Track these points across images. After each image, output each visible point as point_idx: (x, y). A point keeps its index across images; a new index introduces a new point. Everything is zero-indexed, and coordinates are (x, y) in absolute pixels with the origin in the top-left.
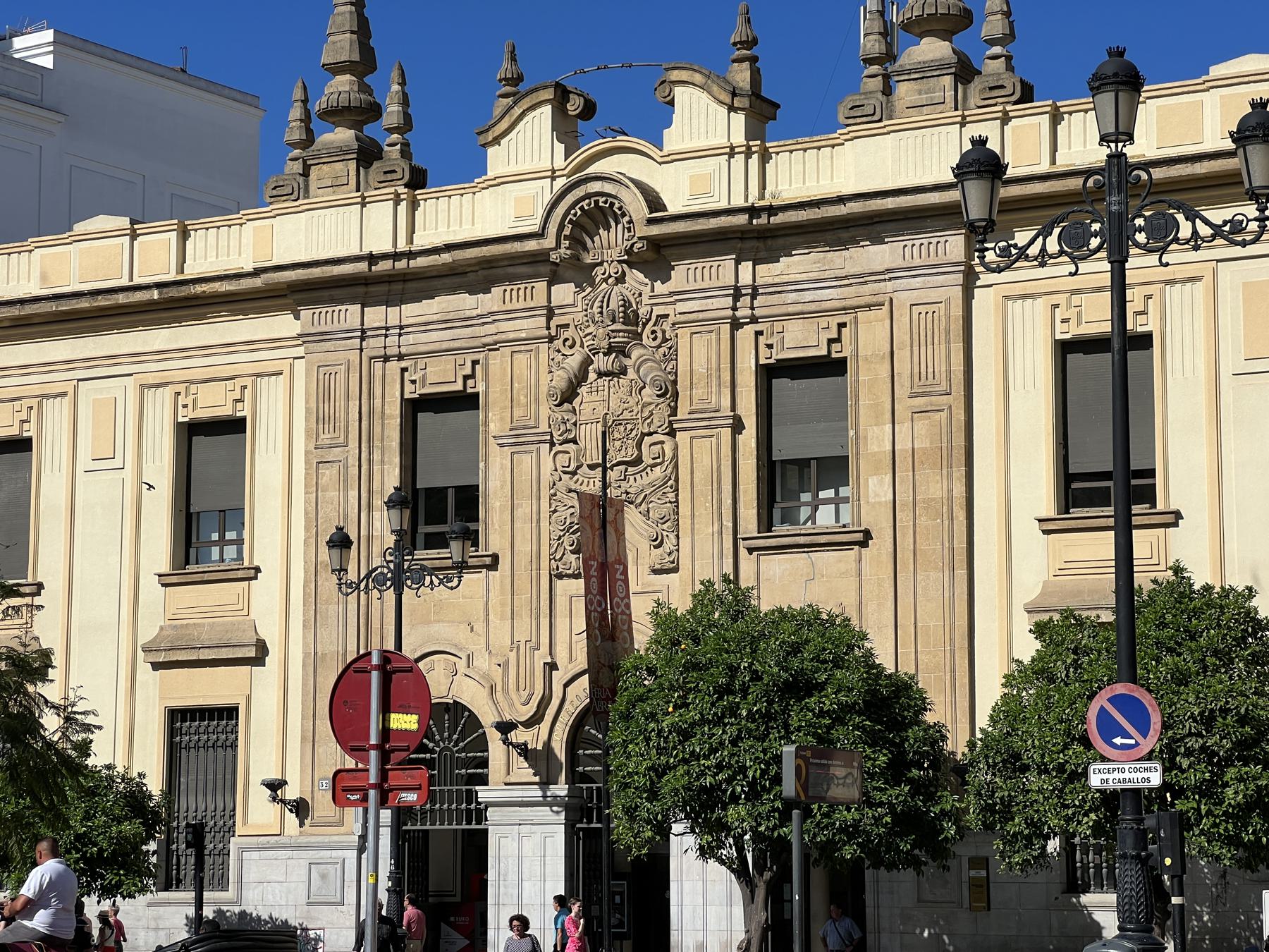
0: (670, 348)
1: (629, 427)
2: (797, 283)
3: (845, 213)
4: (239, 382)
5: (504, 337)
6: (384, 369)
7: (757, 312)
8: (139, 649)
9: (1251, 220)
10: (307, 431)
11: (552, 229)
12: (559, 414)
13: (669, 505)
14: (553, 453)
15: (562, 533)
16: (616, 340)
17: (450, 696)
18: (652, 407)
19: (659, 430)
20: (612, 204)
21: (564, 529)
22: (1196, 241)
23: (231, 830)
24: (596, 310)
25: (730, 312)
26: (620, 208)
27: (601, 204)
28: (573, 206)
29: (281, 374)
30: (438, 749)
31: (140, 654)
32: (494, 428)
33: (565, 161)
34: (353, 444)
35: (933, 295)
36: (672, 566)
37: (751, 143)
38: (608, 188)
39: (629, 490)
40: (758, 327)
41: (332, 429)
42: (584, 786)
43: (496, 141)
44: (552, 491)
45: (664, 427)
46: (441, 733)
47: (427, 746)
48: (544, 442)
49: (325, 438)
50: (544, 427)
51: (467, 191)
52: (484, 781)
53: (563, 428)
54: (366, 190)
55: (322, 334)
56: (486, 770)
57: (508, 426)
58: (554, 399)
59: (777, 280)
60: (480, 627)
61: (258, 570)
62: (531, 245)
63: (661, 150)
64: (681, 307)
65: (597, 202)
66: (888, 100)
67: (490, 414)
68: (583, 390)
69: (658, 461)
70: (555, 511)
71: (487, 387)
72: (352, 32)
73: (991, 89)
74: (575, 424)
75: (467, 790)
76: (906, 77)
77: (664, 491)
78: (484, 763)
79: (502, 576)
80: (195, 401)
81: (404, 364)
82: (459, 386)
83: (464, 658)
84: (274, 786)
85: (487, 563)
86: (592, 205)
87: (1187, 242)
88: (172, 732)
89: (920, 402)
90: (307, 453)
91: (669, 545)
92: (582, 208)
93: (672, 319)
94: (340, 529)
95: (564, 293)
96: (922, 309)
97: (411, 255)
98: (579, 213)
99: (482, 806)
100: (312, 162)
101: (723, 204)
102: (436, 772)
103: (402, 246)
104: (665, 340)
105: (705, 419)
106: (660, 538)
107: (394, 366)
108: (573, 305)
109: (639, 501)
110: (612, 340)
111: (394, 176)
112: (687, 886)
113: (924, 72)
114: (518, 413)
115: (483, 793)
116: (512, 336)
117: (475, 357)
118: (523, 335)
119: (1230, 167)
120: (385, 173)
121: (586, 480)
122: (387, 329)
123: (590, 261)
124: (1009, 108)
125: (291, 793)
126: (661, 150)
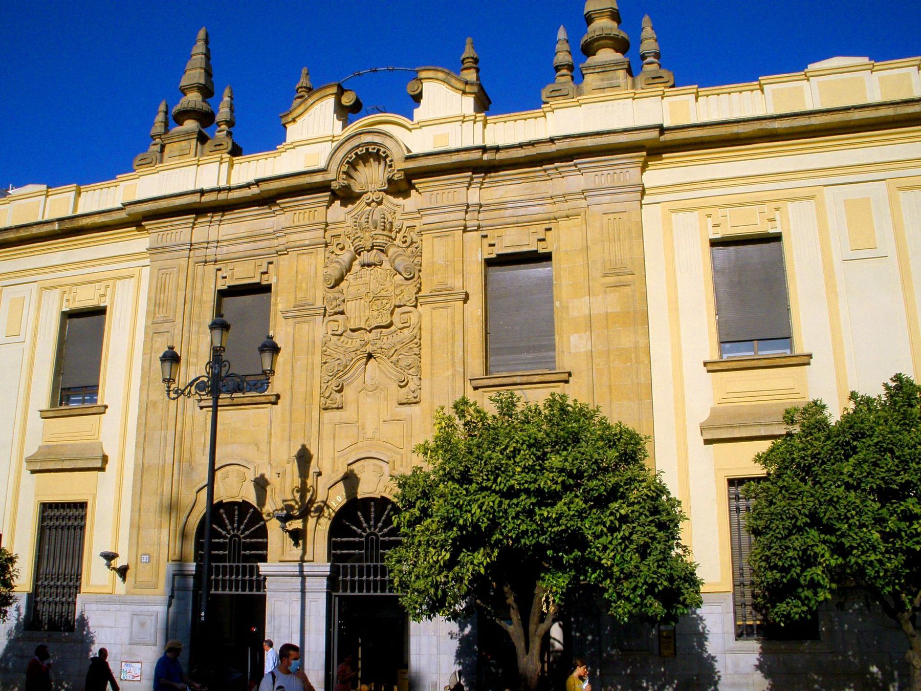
0: (416, 248)
1: (385, 301)
2: (514, 202)
3: (555, 150)
4: (104, 284)
5: (293, 244)
6: (204, 271)
7: (482, 223)
8: (24, 461)
10: (148, 312)
11: (334, 167)
12: (332, 293)
14: (325, 322)
15: (330, 378)
16: (378, 241)
17: (240, 496)
18: (402, 288)
19: (408, 304)
20: (379, 150)
23: (78, 588)
24: (363, 220)
25: (463, 222)
26: (384, 152)
27: (370, 150)
28: (350, 152)
29: (133, 277)
30: (229, 536)
31: (25, 464)
33: (343, 129)
34: (179, 320)
35: (619, 207)
36: (415, 400)
37: (478, 115)
38: (377, 139)
39: (383, 346)
40: (484, 233)
41: (164, 311)
42: (341, 565)
43: (294, 120)
44: (324, 348)
45: (412, 301)
46: (232, 523)
47: (227, 526)
49: (160, 316)
50: (319, 303)
52: (264, 559)
53: (334, 303)
54: (201, 156)
55: (163, 247)
56: (265, 552)
57: (292, 304)
59: (497, 201)
60: (264, 447)
61: (106, 407)
62: (318, 178)
64: (426, 220)
65: (367, 149)
66: (578, 88)
67: (279, 298)
68: (349, 277)
69: (407, 325)
70: (325, 363)
71: (278, 280)
72: (201, 68)
73: (653, 78)
74: (344, 301)
75: (243, 566)
76: (592, 71)
78: (264, 546)
80: (74, 297)
81: (218, 267)
82: (256, 280)
83: (252, 469)
84: (109, 557)
86: (364, 151)
88: (42, 519)
89: (611, 280)
90: (146, 327)
91: (412, 385)
92: (356, 154)
93: (417, 229)
94: (171, 348)
95: (337, 211)
96: (611, 216)
97: (230, 189)
98: (354, 156)
99: (262, 578)
100: (166, 142)
101: (40, 219)
102: (227, 552)
103: (223, 184)
104: (412, 243)
105: (444, 294)
106: (406, 381)
107: (211, 268)
108: (344, 222)
109: (391, 354)
110: (374, 241)
111: (221, 147)
112: (424, 640)
113: (604, 68)
114: (300, 295)
115: (263, 568)
116: (298, 244)
117: (270, 260)
118: (307, 242)
119: (837, 120)
120: (216, 146)
121: (350, 341)
122: (208, 243)
124: (666, 90)
125: (118, 563)
126: (412, 120)
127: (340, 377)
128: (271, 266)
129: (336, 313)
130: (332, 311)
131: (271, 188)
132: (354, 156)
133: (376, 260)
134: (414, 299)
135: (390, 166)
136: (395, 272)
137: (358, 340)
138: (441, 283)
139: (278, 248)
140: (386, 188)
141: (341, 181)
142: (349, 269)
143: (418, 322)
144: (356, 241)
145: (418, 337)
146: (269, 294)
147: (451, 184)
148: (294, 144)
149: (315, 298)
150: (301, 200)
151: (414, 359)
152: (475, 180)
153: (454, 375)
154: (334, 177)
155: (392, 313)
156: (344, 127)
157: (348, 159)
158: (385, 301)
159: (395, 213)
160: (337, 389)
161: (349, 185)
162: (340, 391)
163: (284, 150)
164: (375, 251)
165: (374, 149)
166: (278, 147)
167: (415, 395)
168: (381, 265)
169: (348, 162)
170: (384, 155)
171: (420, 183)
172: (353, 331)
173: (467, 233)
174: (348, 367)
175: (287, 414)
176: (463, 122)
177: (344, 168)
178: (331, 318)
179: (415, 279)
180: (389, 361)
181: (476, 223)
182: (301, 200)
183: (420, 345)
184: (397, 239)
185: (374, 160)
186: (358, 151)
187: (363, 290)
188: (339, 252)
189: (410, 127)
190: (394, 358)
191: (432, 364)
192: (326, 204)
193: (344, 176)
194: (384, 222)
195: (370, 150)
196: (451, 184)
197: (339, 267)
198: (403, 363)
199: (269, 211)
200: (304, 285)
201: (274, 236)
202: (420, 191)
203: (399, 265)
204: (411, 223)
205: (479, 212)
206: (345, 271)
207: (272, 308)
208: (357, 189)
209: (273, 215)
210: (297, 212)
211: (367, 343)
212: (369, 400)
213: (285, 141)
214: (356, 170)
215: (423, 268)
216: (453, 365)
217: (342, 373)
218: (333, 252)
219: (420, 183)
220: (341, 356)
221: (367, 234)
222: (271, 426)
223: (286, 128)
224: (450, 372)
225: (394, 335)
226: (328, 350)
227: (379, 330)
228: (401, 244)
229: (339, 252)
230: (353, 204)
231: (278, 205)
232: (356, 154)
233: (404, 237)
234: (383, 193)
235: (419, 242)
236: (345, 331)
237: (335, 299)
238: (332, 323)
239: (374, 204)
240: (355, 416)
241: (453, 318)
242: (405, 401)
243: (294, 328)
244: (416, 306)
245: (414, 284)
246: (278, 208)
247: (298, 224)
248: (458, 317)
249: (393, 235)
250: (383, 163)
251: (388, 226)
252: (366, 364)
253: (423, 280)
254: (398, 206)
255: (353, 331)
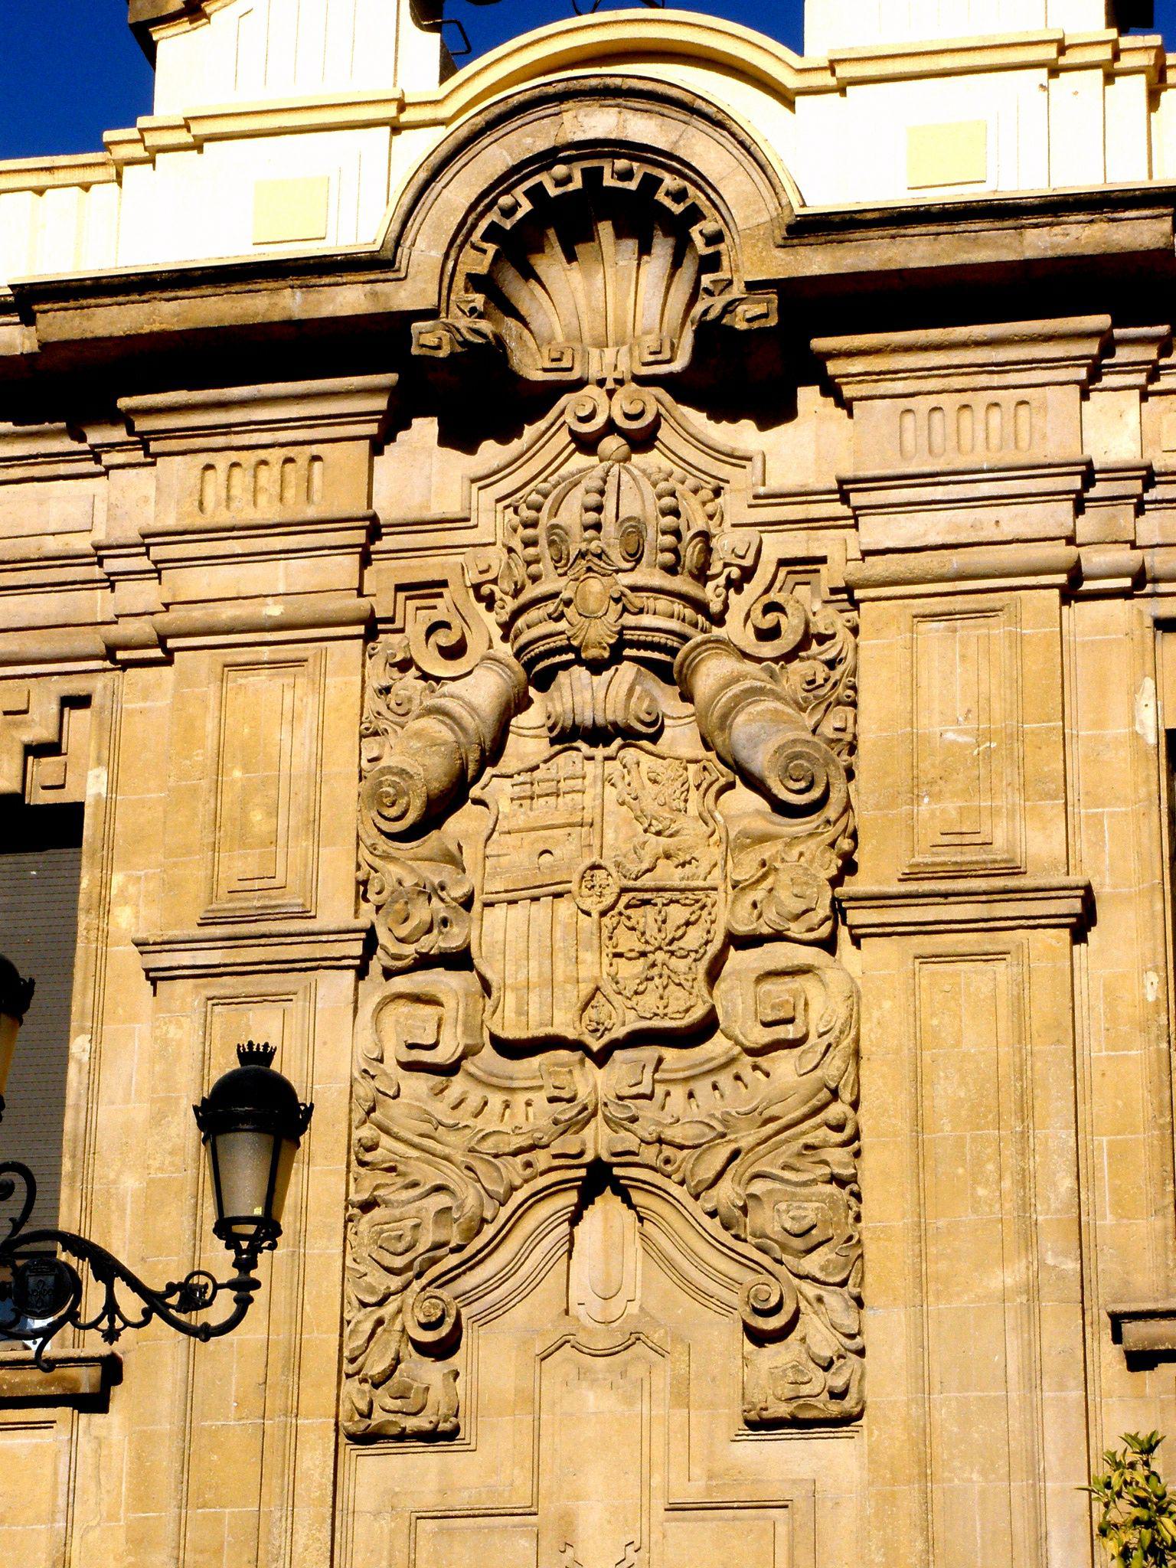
0: (831, 664)
5: (198, 615)
9: (222, 1286)
13: (833, 1188)
15: (395, 1282)
16: (646, 620)
18: (767, 851)
19: (796, 930)
20: (651, 183)
21: (409, 1267)
22: (112, 1321)
24: (571, 515)
25: (1062, 553)
26: (679, 196)
27: (608, 181)
28: (506, 181)
32: (126, 920)
33: (443, 79)
36: (834, 1409)
37: (1125, 42)
39: (668, 1134)
44: (366, 1132)
48: (335, 964)
51: (60, 177)
53: (421, 913)
58: (393, 812)
63: (798, 47)
64: (877, 531)
67: (118, 879)
68: (494, 787)
69: (789, 1032)
70: (367, 1206)
71: (113, 785)
74: (467, 903)
77: (809, 1139)
79: (142, 1443)
85: (85, 1389)
86: (577, 184)
87: (94, 1325)
92: (536, 194)
93: (831, 575)
98: (526, 206)
106: (789, 1308)
108: (462, 521)
110: (629, 620)
114: (237, 866)
116: (227, 613)
118: (274, 610)
121: (496, 1100)
123: (539, 376)
126: (798, 47)
127: (445, 1280)
128: (77, 718)
129: (424, 962)
130: (409, 950)
131: (101, 332)
132: (526, 206)
133: (634, 713)
134: (823, 910)
135: (711, 263)
136: (722, 774)
137: (540, 1098)
138: (957, 838)
139: (116, 632)
140: (677, 366)
141: (463, 323)
142: (493, 753)
143: (848, 1023)
144: (533, 614)
145: (847, 1096)
146: (67, 853)
147: (1002, 368)
148: (200, 129)
149: (313, 883)
150: (243, 403)
151: (833, 1201)
152: (1123, 355)
153: (1032, 1291)
154: (429, 301)
155: (714, 974)
156: (448, 69)
157: (493, 216)
158: (677, 914)
159: (717, 492)
160: (429, 1337)
161: (499, 339)
162: (444, 1349)
163: (138, 151)
164: (627, 671)
165: (627, 175)
166: (108, 136)
167: (838, 1383)
168: (654, 738)
169: (493, 233)
170: (677, 209)
171: (850, 354)
172: (512, 1049)
173: (1078, 607)
174: (489, 1231)
175: (165, 1459)
176: (1055, 71)
177: (477, 262)
178: (400, 984)
179: (831, 811)
180: (696, 1208)
181: (1127, 558)
182: (243, 403)
183: (856, 1136)
184: (734, 618)
185: (620, 234)
186: (544, 178)
187: (570, 853)
188: (439, 667)
189: (791, 81)
190: (727, 1193)
191: (921, 1235)
192: (372, 429)
193: (479, 300)
194: (677, 533)
195: (608, 181)
196: (1002, 368)
197: (447, 735)
198: (770, 1220)
199: (67, 445)
200: (257, 816)
201: (96, 572)
202: (848, 392)
203: (754, 741)
204: (796, 544)
205: (1140, 510)
206: (474, 756)
207: (83, 920)
208: (532, 366)
209: (90, 467)
210: (222, 461)
211: (585, 1116)
212: (594, 1400)
213: (149, 110)
214: (529, 274)
215: (863, 762)
216: (1029, 1237)
217: (454, 1259)
218: (405, 665)
219: (850, 354)
220: (452, 1176)
221: (595, 585)
222: (70, 1521)
223: (150, 50)
224: (1011, 1276)
225: (724, 1079)
226: (385, 1140)
227: (649, 1053)
228: (746, 639)
229: (439, 667)
230: (504, 439)
231: (125, 418)
232: (536, 194)
233: (772, 607)
234: (659, 392)
235: (844, 635)
236: (468, 1053)
237: (430, 892)
238: (403, 1008)
239: (612, 444)
240: (521, 1478)
241: (1019, 1009)
242: (783, 1410)
243: (206, 1027)
244: (829, 945)
245: (827, 837)
246: (119, 434)
247: (224, 518)
248: (1045, 1003)
249: (711, 594)
250: (662, 248)
251: (691, 554)
252: (575, 1219)
253: (863, 817)
254: (739, 459)
255: (512, 1049)
